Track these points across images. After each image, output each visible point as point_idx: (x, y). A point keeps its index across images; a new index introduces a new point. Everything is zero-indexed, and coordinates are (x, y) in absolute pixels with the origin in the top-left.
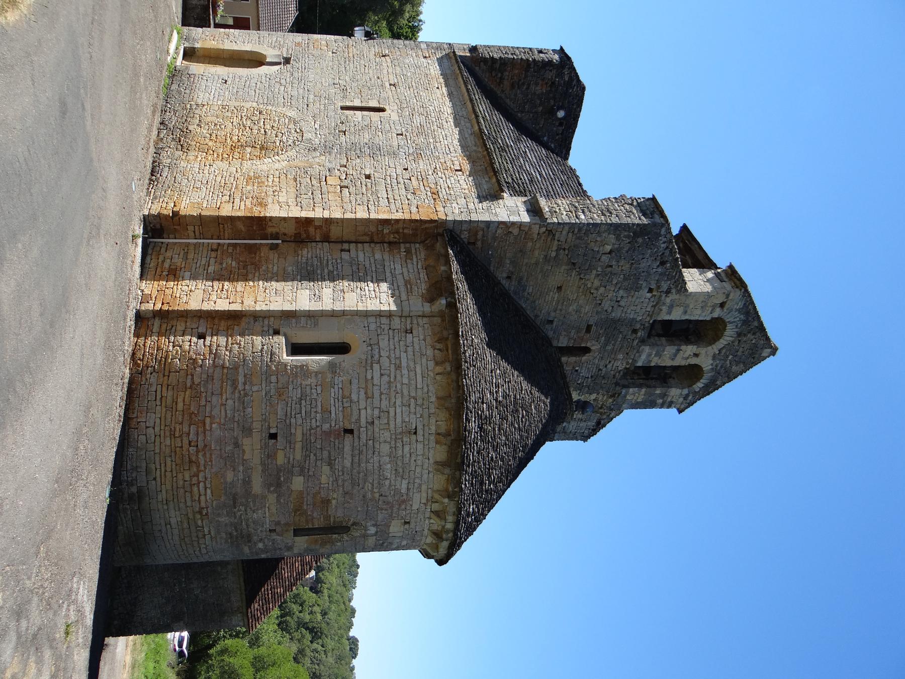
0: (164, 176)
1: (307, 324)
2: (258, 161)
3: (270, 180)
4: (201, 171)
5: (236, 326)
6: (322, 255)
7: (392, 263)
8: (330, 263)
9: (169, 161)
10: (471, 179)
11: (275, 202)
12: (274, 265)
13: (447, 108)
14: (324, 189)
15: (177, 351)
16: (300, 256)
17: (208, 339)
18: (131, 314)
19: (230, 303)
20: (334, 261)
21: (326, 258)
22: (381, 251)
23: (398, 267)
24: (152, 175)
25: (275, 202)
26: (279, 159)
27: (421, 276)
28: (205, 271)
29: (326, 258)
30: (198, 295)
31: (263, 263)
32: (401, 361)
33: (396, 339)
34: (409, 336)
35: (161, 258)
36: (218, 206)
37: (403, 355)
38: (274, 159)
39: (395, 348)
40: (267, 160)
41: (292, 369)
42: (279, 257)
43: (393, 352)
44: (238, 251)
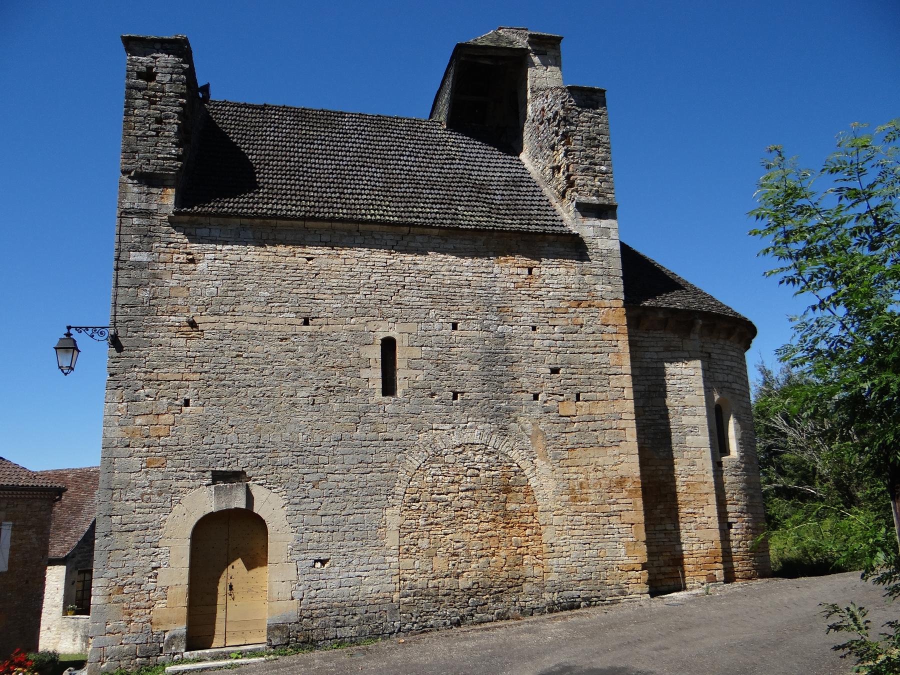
0: (578, 593)
7: (644, 360)
8: (650, 417)
10: (544, 261)
13: (380, 256)
15: (744, 544)
17: (730, 520)
18: (659, 603)
21: (644, 421)
23: (648, 355)
24: (578, 607)
27: (658, 335)
29: (644, 421)
33: (716, 367)
35: (661, 577)
40: (533, 483)
41: (742, 452)
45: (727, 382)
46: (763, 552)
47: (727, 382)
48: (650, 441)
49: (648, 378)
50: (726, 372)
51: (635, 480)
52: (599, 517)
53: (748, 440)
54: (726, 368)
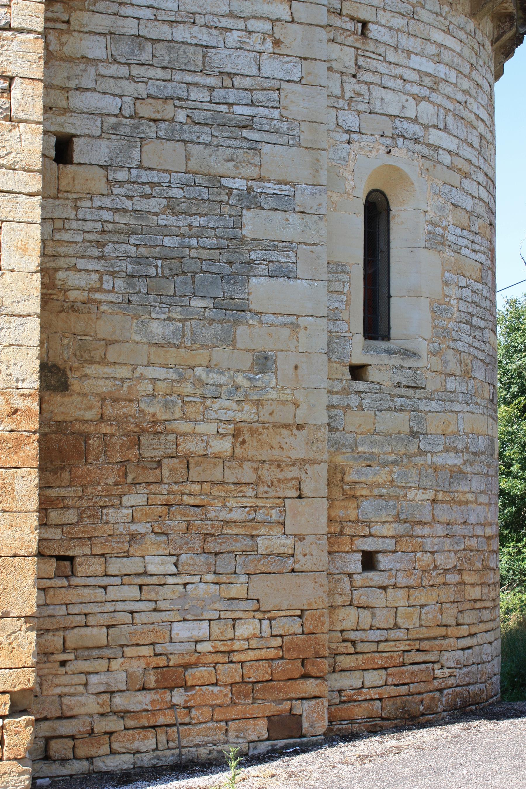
1: (341, 293)
5: (347, 478)
6: (89, 226)
8: (128, 204)
12: (142, 377)
16: (98, 296)
19: (300, 497)
20: (117, 190)
21: (106, 215)
22: (69, 32)
28: (171, 580)
29: (106, 215)
30: (365, 76)
31: (131, 409)
32: (430, 75)
33: (382, 68)
34: (373, 30)
37: (416, 62)
39: (401, 78)
42: (103, 361)
43: (408, 86)
44: (69, 492)
45: (415, 120)
46: (471, 635)
47: (415, 120)
48: (120, 283)
49: (136, 71)
50: (416, 89)
51: (19, 404)
53: (463, 306)
54: (415, 77)
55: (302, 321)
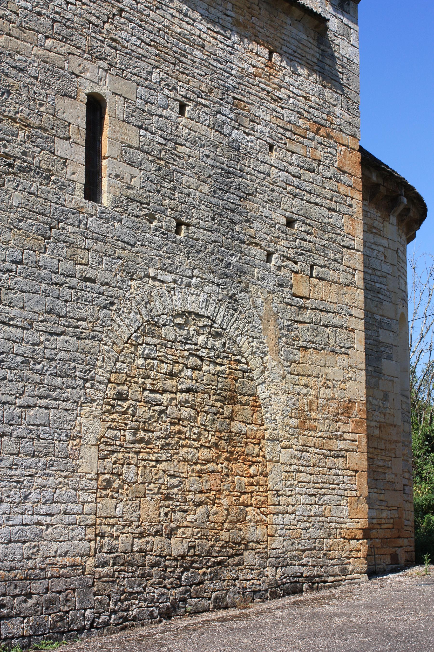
2: (263, 410)
3: (305, 391)
4: (290, 509)
9: (269, 571)
11: (343, 386)
14: (317, 304)
25: (343, 386)
26: (259, 370)
36: (354, 474)
38: (260, 381)
52: (326, 456)
55: (395, 379)
